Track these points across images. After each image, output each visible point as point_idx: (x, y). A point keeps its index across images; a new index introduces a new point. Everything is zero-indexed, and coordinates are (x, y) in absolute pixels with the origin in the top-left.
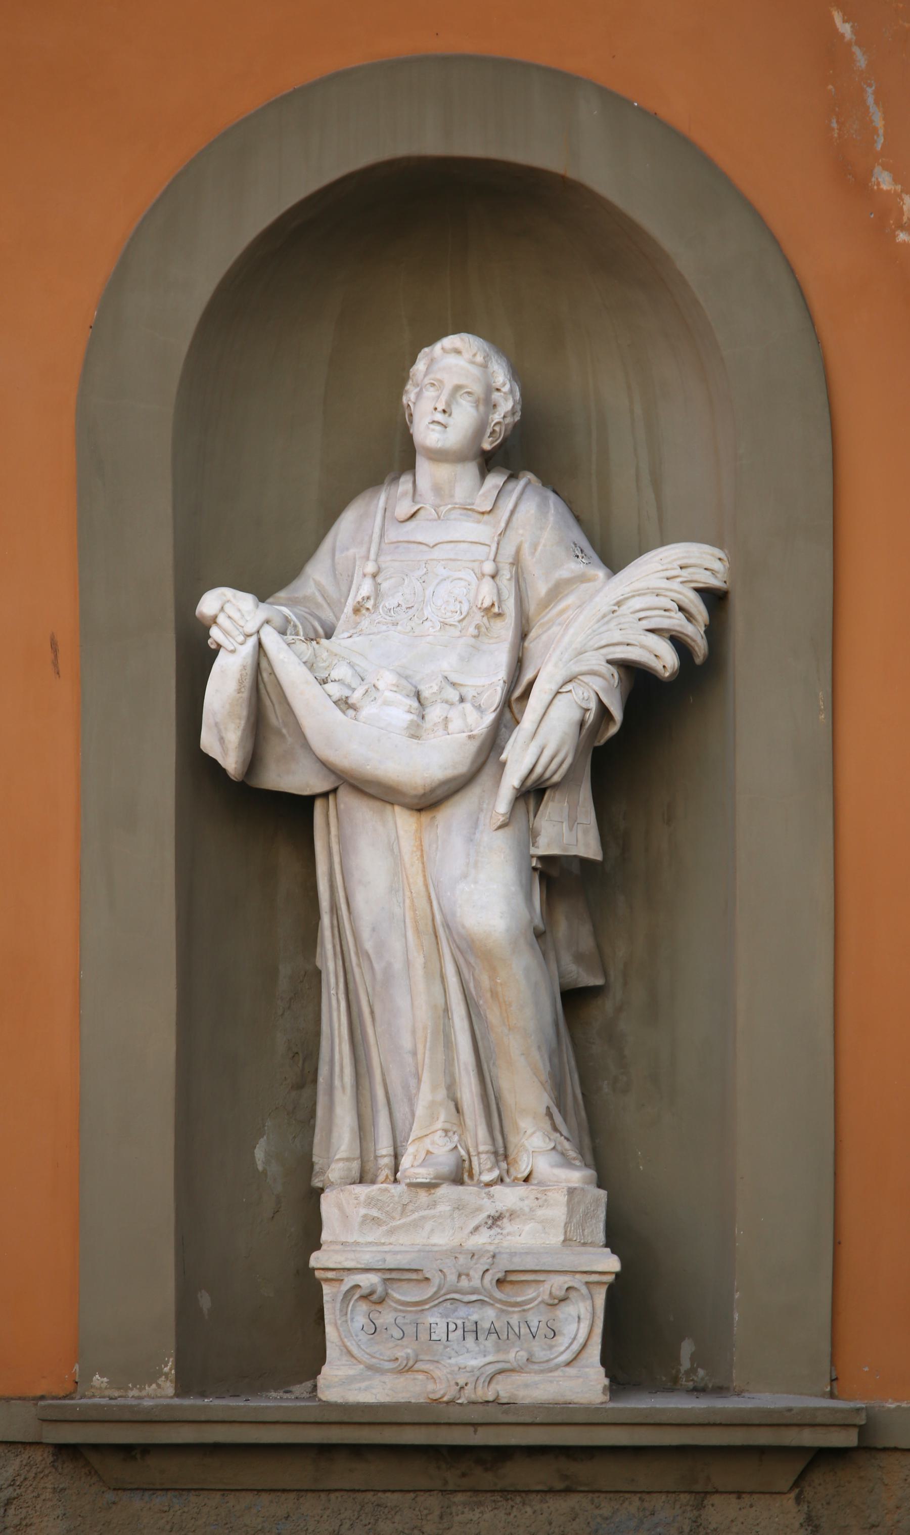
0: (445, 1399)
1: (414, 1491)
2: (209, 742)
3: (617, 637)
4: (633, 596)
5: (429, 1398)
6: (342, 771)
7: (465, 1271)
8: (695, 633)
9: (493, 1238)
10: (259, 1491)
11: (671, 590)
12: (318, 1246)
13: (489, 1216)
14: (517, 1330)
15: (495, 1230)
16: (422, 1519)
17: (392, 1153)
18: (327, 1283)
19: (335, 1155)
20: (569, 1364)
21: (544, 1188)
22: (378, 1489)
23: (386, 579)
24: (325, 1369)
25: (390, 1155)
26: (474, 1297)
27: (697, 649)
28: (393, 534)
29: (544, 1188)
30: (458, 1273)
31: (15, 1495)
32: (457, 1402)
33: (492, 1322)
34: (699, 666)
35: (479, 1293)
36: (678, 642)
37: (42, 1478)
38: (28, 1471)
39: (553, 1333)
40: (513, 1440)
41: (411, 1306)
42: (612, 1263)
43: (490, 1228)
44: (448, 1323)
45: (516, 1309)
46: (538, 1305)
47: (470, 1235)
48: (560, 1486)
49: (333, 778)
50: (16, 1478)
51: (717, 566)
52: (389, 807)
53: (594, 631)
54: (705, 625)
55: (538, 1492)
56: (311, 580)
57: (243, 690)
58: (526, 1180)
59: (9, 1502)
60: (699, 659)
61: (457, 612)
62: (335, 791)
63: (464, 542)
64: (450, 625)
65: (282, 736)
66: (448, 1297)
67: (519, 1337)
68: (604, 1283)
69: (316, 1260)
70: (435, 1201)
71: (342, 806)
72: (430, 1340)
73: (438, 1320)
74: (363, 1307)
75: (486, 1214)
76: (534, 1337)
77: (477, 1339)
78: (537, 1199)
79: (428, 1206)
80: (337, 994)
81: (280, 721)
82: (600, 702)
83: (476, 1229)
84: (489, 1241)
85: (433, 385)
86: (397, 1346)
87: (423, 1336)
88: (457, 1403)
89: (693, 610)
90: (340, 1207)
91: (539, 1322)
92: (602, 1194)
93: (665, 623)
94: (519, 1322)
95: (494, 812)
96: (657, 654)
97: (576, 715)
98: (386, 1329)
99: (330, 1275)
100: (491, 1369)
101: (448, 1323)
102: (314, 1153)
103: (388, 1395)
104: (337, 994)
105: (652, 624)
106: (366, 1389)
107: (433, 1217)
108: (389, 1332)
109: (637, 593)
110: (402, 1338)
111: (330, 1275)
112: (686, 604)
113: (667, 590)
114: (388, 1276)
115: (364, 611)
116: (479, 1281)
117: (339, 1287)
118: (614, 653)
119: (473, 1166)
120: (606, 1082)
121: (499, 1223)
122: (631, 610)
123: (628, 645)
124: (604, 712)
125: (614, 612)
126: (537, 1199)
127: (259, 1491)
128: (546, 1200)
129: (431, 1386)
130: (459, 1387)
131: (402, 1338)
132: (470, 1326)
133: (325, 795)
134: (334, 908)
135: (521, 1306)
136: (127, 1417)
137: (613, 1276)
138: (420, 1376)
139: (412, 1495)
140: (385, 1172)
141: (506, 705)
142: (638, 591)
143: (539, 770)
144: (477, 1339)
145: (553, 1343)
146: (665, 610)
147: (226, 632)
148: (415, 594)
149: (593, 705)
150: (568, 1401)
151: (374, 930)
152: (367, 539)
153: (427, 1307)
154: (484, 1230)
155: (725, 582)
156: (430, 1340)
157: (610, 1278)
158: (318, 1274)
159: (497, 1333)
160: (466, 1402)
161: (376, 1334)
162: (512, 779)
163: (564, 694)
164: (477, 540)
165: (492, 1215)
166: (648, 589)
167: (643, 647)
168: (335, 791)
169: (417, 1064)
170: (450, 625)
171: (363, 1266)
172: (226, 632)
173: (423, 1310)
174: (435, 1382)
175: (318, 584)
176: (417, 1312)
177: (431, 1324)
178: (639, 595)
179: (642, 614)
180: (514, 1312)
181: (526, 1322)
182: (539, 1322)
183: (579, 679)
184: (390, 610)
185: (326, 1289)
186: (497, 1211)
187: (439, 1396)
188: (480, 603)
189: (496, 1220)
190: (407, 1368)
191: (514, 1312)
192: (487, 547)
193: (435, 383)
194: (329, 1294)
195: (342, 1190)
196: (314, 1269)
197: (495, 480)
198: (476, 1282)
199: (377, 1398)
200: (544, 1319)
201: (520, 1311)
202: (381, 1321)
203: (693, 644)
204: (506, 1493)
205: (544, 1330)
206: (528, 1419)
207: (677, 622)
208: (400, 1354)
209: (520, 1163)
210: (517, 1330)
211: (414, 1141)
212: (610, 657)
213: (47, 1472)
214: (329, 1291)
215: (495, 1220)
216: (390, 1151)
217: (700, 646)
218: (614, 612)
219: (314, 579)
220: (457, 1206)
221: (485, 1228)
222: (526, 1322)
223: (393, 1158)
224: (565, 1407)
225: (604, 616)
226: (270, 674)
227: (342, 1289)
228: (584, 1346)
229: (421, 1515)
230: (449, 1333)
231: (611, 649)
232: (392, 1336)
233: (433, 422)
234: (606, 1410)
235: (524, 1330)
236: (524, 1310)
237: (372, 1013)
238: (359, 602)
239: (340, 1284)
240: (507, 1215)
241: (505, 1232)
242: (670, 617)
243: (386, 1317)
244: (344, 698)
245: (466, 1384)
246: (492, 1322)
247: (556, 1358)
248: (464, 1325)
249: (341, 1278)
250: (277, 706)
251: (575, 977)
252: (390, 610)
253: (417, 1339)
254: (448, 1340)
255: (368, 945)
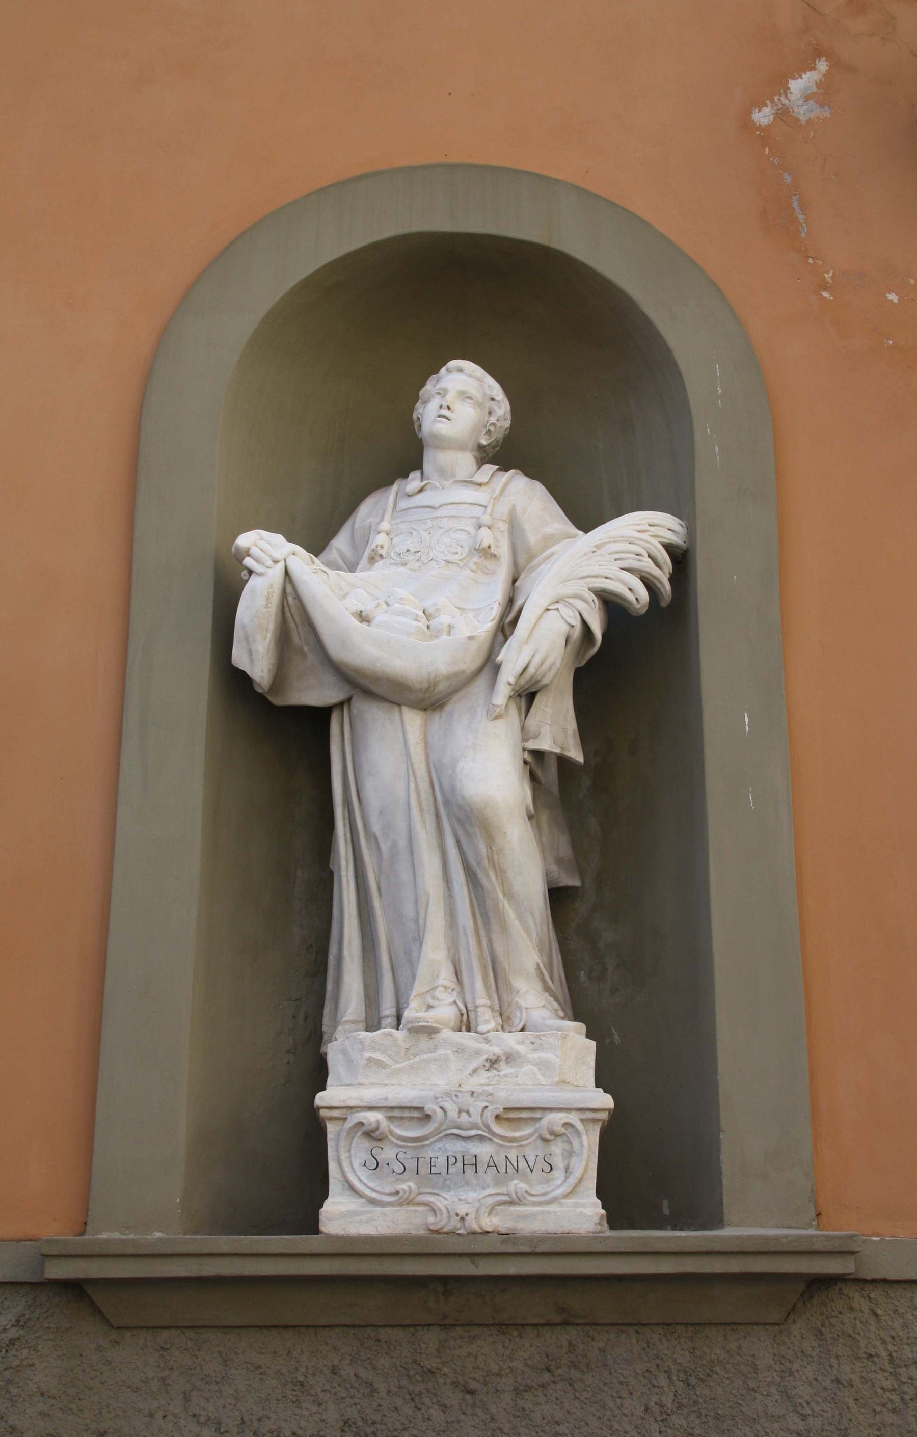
0: (445, 1230)
1: (414, 1326)
2: (239, 658)
3: (597, 570)
4: (609, 542)
5: (429, 1229)
6: (357, 671)
7: (465, 1108)
8: (663, 576)
9: (490, 1079)
10: (260, 1327)
11: (641, 540)
12: (323, 1088)
13: (487, 1059)
14: (515, 1164)
15: (493, 1072)
16: (421, 1353)
17: (395, 1014)
18: (331, 1122)
19: (342, 1017)
20: (567, 1196)
21: (539, 1033)
22: (378, 1324)
23: (396, 536)
24: (327, 1203)
25: (393, 1016)
26: (473, 1132)
27: (662, 590)
28: (404, 504)
29: (539, 1033)
30: (458, 1110)
31: (17, 1335)
32: (457, 1232)
33: (491, 1156)
34: (582, 885)
35: (478, 1128)
36: (647, 582)
37: (46, 1318)
38: (32, 1312)
39: (549, 1166)
40: (512, 1269)
41: (412, 1142)
42: (606, 1101)
43: (488, 1070)
44: (448, 1157)
45: (514, 1144)
46: (535, 1140)
47: (469, 1076)
48: (558, 1319)
49: (347, 687)
50: (20, 1319)
51: (677, 528)
52: (396, 708)
53: (577, 565)
54: (669, 574)
55: (535, 1325)
56: (333, 548)
57: (270, 605)
58: (522, 1030)
59: (12, 1342)
60: (664, 604)
61: (458, 553)
62: (349, 700)
63: (464, 503)
64: (452, 563)
65: (304, 654)
66: (448, 1132)
67: (517, 1171)
68: (598, 1120)
69: (321, 1099)
70: (435, 1045)
71: (355, 711)
72: (431, 1173)
73: (438, 1154)
74: (367, 1144)
75: (485, 1057)
76: (532, 1171)
77: (476, 1172)
78: (532, 1043)
79: (429, 1050)
80: (347, 875)
81: (303, 639)
82: (584, 623)
83: (475, 1071)
84: (487, 1082)
85: (439, 394)
86: (398, 1180)
87: (424, 1170)
88: (458, 1234)
89: (660, 558)
90: (345, 1053)
91: (537, 1156)
92: (593, 1044)
93: (636, 564)
94: (517, 1156)
95: (491, 705)
96: (631, 588)
97: (565, 628)
98: (388, 1164)
99: (335, 1113)
100: (490, 1201)
101: (448, 1157)
102: (323, 1023)
103: (388, 1227)
104: (347, 875)
105: (625, 564)
106: (368, 1221)
107: (435, 1060)
108: (391, 1167)
109: (613, 540)
110: (404, 1172)
111: (335, 1113)
112: (655, 552)
113: (638, 539)
114: (390, 1114)
115: (378, 558)
116: (479, 1118)
117: (343, 1125)
118: (595, 583)
119: (471, 1020)
120: (582, 972)
121: (495, 1066)
122: (608, 552)
123: (606, 578)
124: (587, 629)
125: (594, 552)
126: (532, 1043)
127: (260, 1327)
128: (541, 1044)
129: (431, 1219)
130: (459, 1217)
131: (404, 1172)
132: (469, 1160)
133: (340, 705)
134: (347, 802)
135: (518, 1141)
136: (131, 1250)
137: (607, 1113)
138: (421, 1209)
139: (412, 1330)
140: (391, 1020)
141: (500, 630)
142: (613, 538)
143: (531, 670)
144: (476, 1172)
145: (550, 1177)
146: (637, 555)
147: (257, 560)
148: (421, 542)
149: (577, 623)
150: (567, 1232)
151: (381, 813)
152: (380, 512)
153: (427, 1142)
154: (482, 1072)
155: (685, 542)
156: (431, 1173)
157: (604, 1116)
158: (323, 1113)
159: (496, 1166)
160: (465, 1233)
161: (378, 1169)
162: (508, 675)
163: (552, 611)
164: (475, 502)
165: (490, 1058)
166: (622, 537)
167: (620, 580)
168: (349, 700)
169: (418, 930)
170: (452, 563)
171: (365, 1104)
172: (257, 560)
173: (423, 1146)
174: (435, 1214)
175: (339, 551)
176: (416, 1148)
177: (431, 1158)
178: (614, 542)
179: (618, 556)
180: (511, 1147)
181: (524, 1156)
182: (537, 1156)
183: (564, 601)
184: (400, 554)
185: (331, 1128)
186: (494, 1055)
187: (440, 1227)
188: (478, 544)
189: (493, 1063)
190: (407, 1201)
191: (511, 1147)
192: (483, 508)
193: (441, 392)
194: (333, 1132)
195: (347, 1038)
196: (319, 1108)
197: (490, 468)
198: (476, 1118)
199: (378, 1230)
200: (541, 1155)
201: (517, 1146)
202: (383, 1156)
203: (659, 585)
204: (504, 1327)
205: (541, 1164)
206: (527, 1249)
207: (648, 565)
208: (403, 1187)
209: (513, 1019)
210: (515, 1164)
211: (416, 996)
212: (591, 585)
213: (51, 1312)
214: (333, 1130)
215: (493, 1063)
216: (393, 1011)
217: (666, 587)
218: (594, 552)
219: (335, 548)
220: (457, 1050)
221: (483, 1070)
222: (524, 1156)
223: (395, 1019)
224: (566, 1237)
225: (586, 554)
226: (295, 598)
227: (345, 1126)
228: (580, 1181)
229: (420, 1349)
230: (449, 1166)
231: (593, 579)
232: (393, 1171)
233: (440, 416)
234: (605, 1239)
235: (522, 1164)
236: (521, 1145)
237: (379, 889)
238: (373, 550)
239: (344, 1122)
240: (504, 1058)
241: (502, 1073)
242: (640, 560)
243: (387, 1153)
244: (358, 611)
245: (467, 1215)
246: (491, 1156)
247: (553, 1190)
248: (463, 1158)
249: (345, 1116)
250: (300, 627)
251: (556, 876)
252: (400, 554)
253: (418, 1173)
254: (448, 1173)
255: (376, 828)
